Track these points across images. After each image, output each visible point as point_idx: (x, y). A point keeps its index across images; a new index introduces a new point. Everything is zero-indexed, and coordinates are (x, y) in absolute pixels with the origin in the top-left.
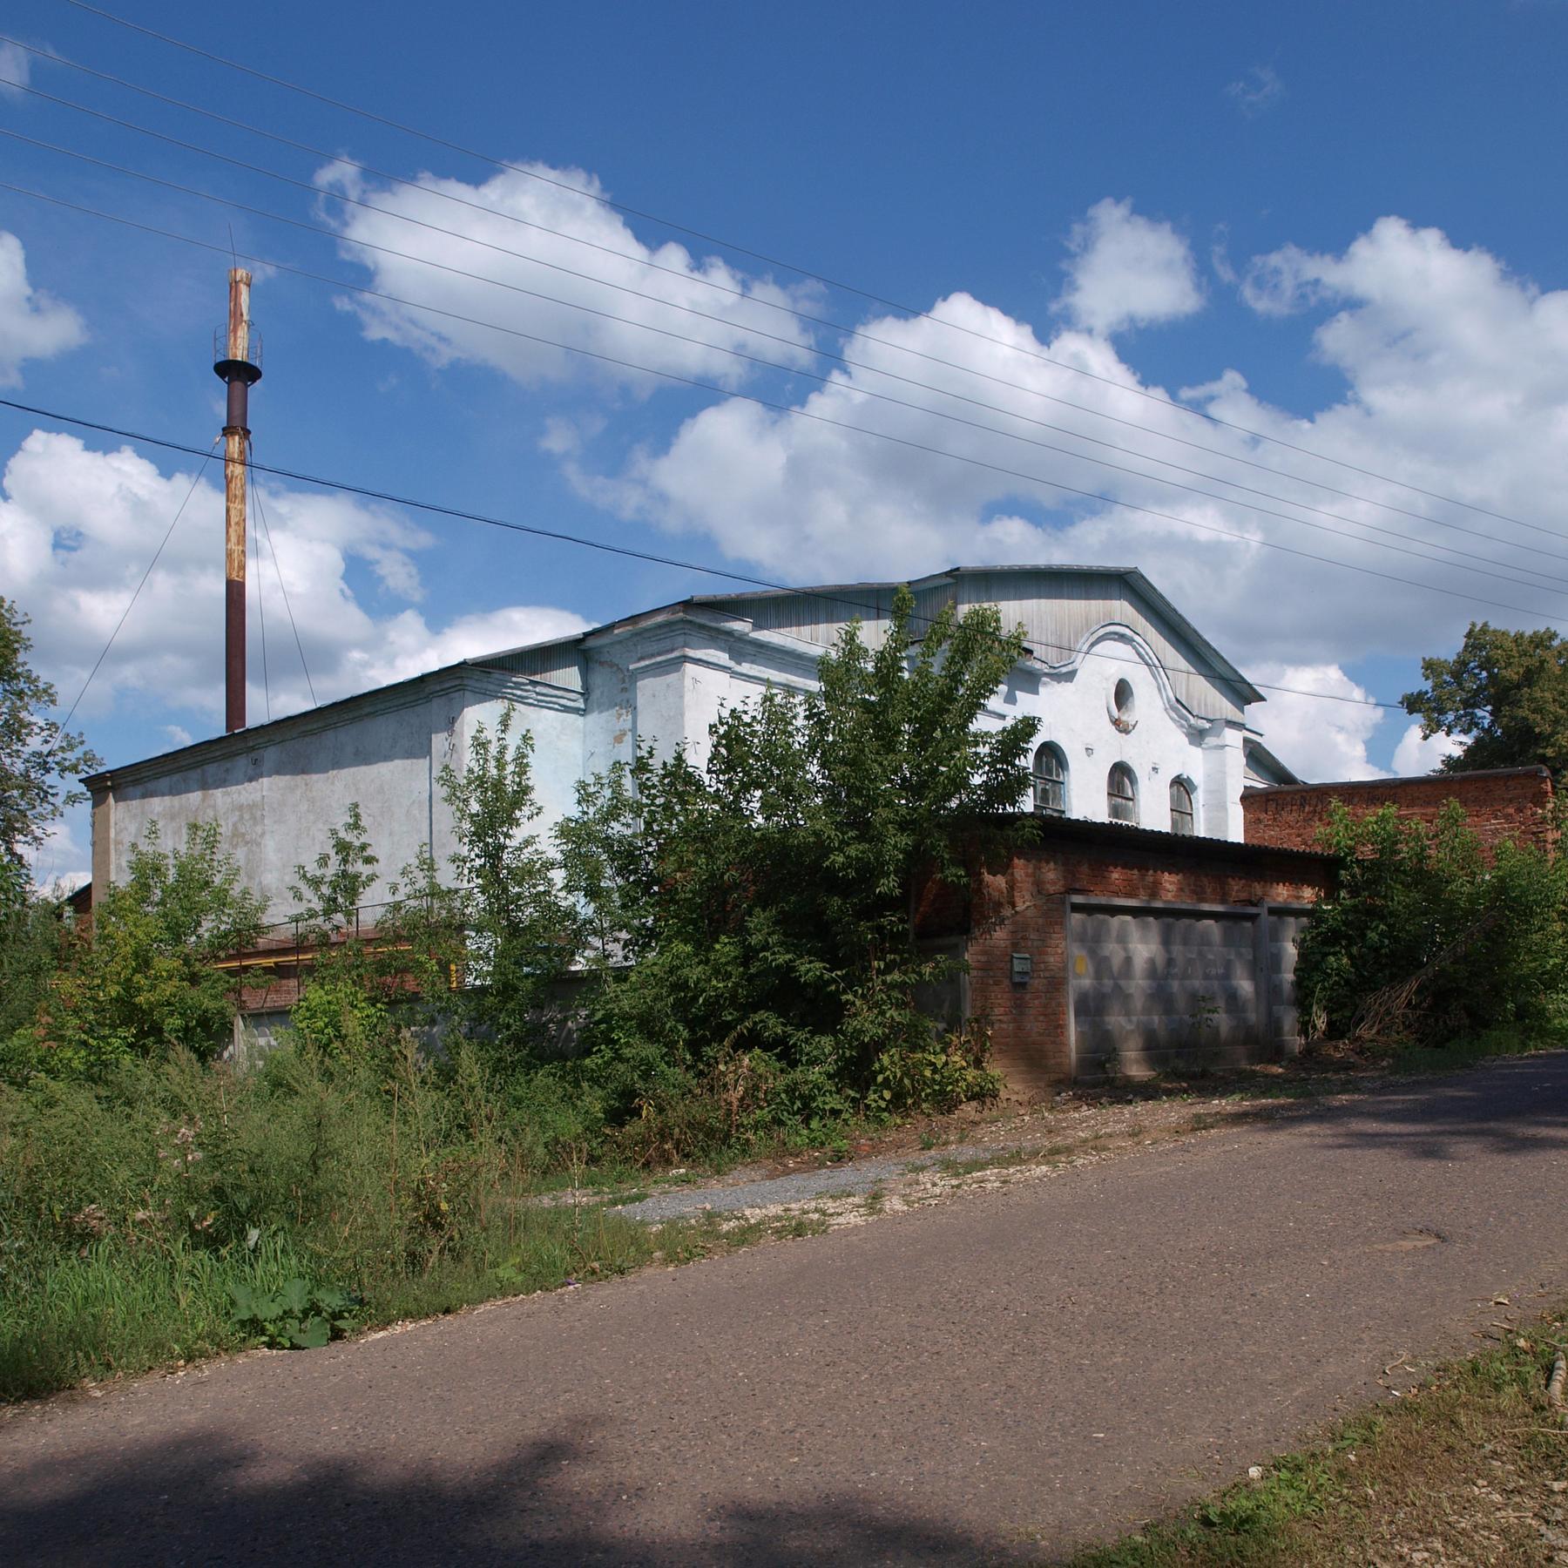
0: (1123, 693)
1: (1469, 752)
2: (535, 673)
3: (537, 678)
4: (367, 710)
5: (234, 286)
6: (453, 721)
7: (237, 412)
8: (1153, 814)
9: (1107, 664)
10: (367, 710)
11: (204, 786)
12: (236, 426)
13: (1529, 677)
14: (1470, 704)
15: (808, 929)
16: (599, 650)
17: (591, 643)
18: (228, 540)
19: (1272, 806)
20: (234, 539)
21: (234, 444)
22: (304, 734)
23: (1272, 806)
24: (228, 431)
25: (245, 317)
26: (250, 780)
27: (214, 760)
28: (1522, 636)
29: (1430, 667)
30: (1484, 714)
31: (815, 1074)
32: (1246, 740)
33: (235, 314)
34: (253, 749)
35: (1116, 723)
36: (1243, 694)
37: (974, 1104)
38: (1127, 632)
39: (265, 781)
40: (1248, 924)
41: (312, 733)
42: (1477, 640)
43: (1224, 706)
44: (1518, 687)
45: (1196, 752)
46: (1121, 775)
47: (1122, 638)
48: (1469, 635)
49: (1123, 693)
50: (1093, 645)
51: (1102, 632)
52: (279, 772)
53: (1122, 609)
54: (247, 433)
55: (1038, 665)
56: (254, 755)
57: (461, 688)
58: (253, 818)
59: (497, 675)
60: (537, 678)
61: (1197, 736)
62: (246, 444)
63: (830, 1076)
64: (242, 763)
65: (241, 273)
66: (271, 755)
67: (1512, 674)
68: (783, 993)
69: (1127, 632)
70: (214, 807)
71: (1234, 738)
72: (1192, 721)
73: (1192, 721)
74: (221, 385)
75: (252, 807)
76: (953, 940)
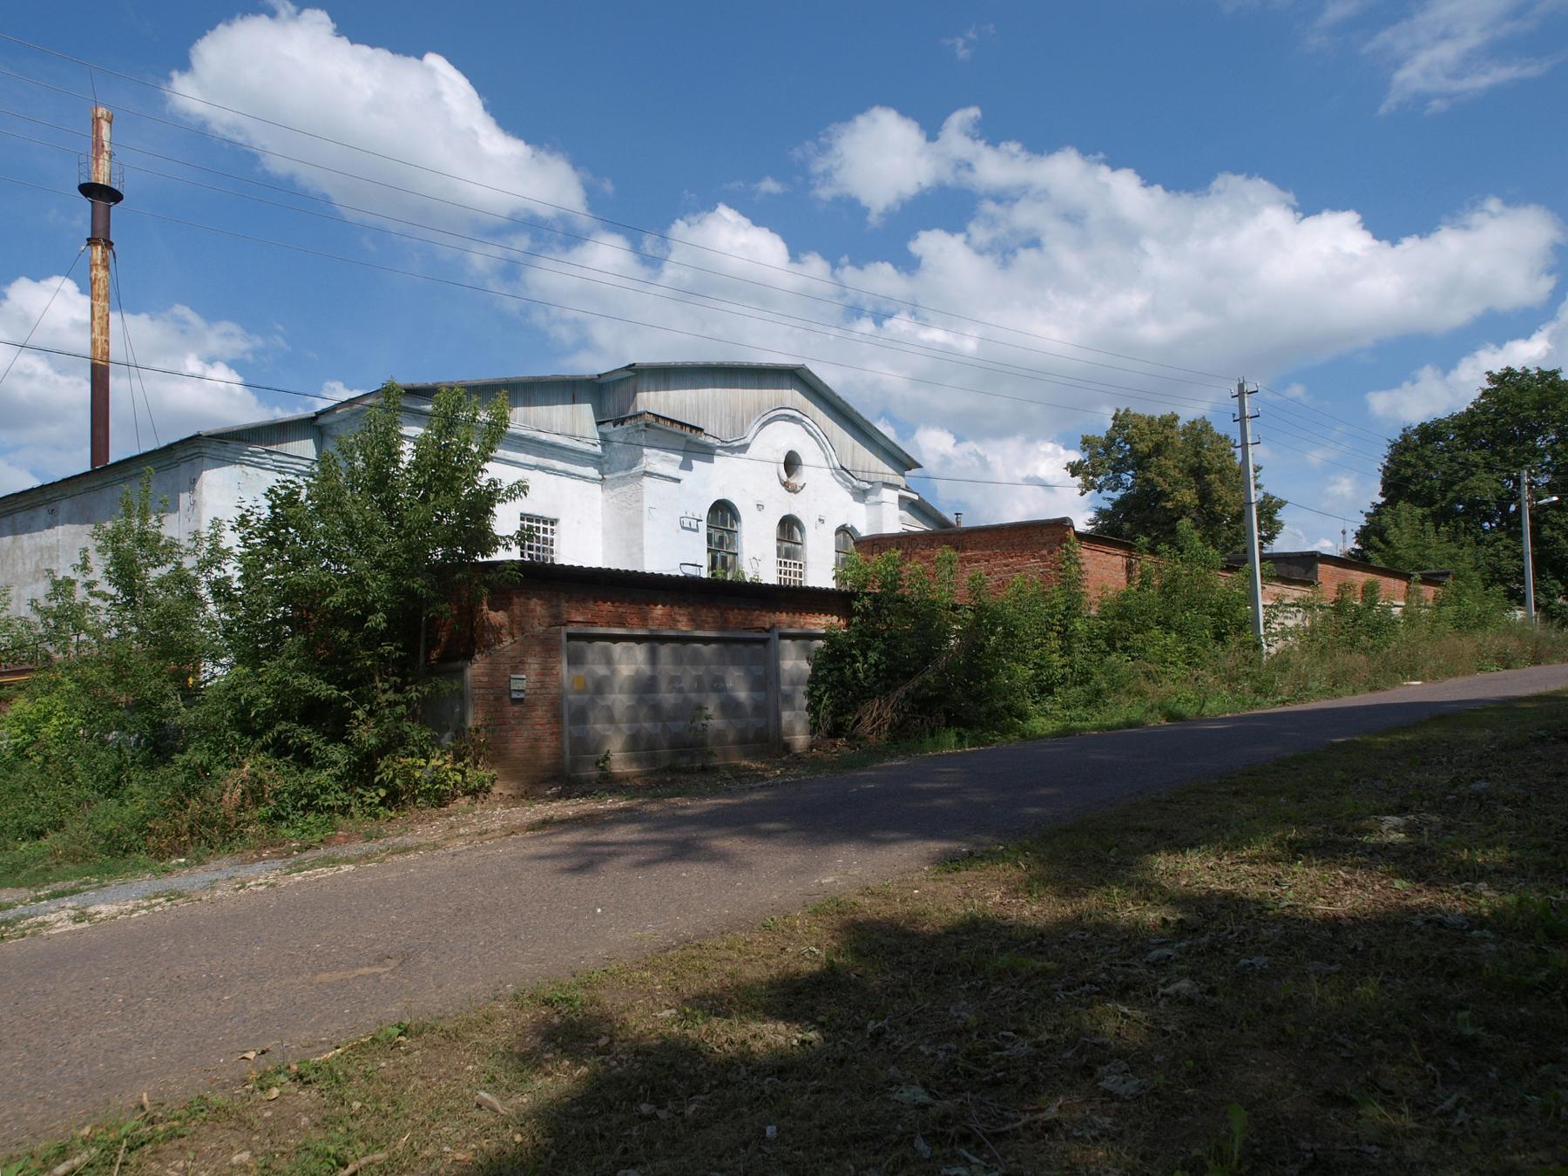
0: (792, 463)
1: (1116, 505)
2: (271, 444)
3: (274, 448)
4: (134, 471)
5: (96, 121)
6: (194, 482)
7: (101, 225)
8: (759, 562)
9: (785, 437)
10: (134, 471)
11: (15, 532)
12: (100, 237)
13: (1158, 450)
14: (1118, 468)
15: (334, 664)
16: (330, 426)
17: (322, 421)
18: (93, 331)
19: (876, 548)
20: (97, 330)
21: (98, 253)
22: (88, 490)
23: (876, 548)
24: (92, 241)
25: (107, 148)
26: (49, 527)
27: (23, 509)
28: (1153, 419)
29: (1087, 443)
30: (1127, 478)
31: (323, 777)
32: (901, 498)
33: (98, 145)
34: (50, 501)
35: (785, 484)
36: (903, 462)
37: (468, 798)
38: (797, 414)
39: (60, 528)
40: (759, 647)
41: (93, 489)
42: (1121, 421)
43: (886, 471)
44: (1149, 456)
45: (861, 507)
46: (789, 527)
47: (792, 419)
48: (1115, 418)
49: (792, 463)
50: (764, 424)
51: (773, 414)
52: (70, 522)
53: (793, 397)
54: (109, 244)
55: (710, 440)
56: (50, 507)
57: (200, 455)
58: (50, 557)
59: (233, 445)
60: (274, 448)
61: (861, 495)
62: (110, 253)
63: (339, 779)
64: (43, 512)
65: (102, 111)
66: (64, 506)
67: (1142, 447)
68: (315, 713)
69: (797, 414)
70: (21, 548)
71: (890, 496)
72: (855, 483)
73: (855, 483)
74: (86, 203)
75: (50, 548)
76: (459, 664)
